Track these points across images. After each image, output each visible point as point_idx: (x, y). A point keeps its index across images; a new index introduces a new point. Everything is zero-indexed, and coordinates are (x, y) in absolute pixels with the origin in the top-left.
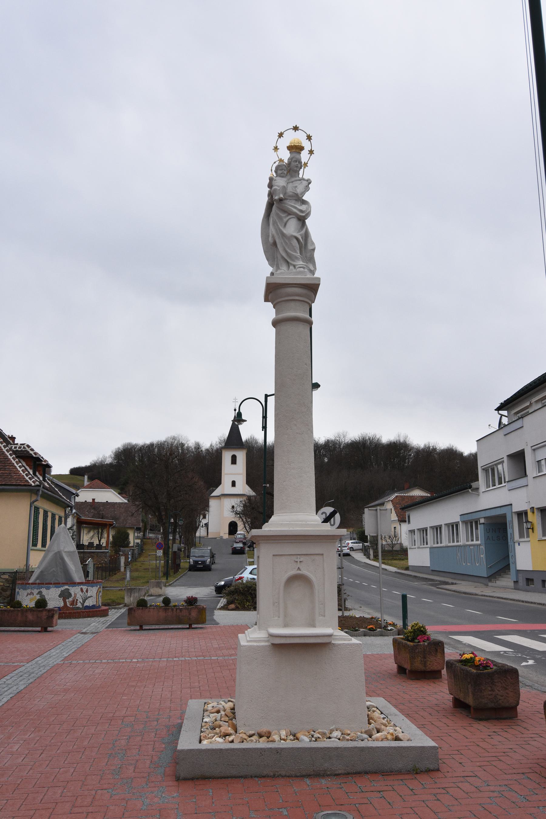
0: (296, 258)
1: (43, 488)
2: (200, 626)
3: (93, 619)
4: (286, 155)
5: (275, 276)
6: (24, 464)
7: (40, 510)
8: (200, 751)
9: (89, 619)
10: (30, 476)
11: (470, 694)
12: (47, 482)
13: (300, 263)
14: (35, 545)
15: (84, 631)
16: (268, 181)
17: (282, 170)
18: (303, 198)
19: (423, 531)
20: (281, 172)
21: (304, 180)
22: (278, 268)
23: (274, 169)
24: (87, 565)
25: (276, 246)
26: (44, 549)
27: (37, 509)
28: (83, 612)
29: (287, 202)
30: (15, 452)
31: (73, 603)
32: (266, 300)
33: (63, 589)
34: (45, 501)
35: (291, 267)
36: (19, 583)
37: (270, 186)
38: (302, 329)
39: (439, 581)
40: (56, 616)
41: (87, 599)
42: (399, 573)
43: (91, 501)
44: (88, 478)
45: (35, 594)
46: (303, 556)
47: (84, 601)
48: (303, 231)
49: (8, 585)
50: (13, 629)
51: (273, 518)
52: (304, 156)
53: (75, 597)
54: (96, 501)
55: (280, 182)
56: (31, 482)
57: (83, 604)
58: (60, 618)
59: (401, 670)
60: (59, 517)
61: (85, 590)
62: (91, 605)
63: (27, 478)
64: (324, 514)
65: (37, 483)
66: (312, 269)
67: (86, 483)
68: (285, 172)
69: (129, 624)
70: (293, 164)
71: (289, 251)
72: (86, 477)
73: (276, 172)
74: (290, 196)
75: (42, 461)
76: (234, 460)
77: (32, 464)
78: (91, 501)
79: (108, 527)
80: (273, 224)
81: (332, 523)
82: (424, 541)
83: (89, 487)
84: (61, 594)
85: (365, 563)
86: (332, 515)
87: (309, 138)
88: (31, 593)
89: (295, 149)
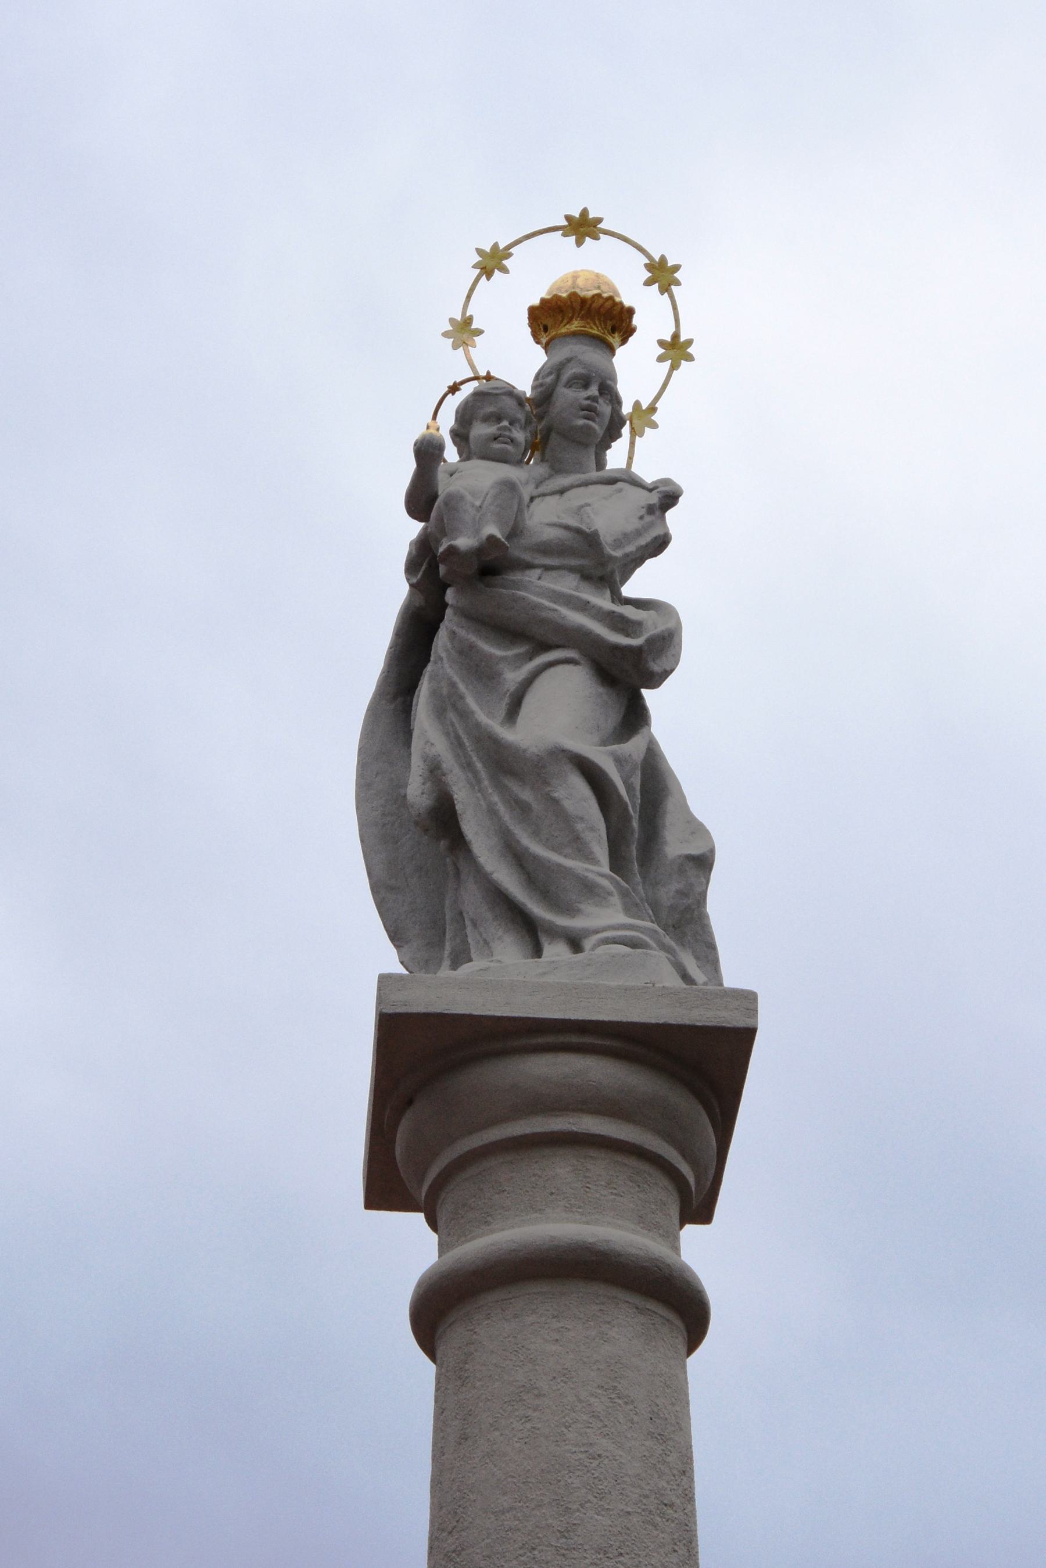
0: (590, 889)
4: (519, 362)
13: (606, 916)
17: (499, 418)
20: (491, 429)
21: (636, 482)
25: (458, 842)
37: (421, 500)
38: (623, 1329)
70: (567, 396)
71: (537, 849)
74: (545, 549)
80: (439, 713)
87: (662, 275)
89: (581, 320)
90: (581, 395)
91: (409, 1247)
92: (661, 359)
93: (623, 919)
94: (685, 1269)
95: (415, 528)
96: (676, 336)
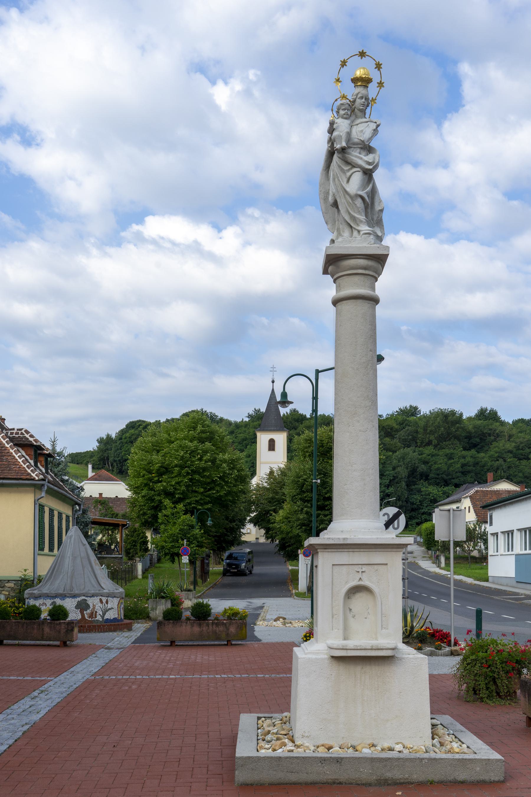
1: (48, 482)
2: (240, 642)
3: (115, 634)
5: (336, 244)
6: (24, 454)
7: (45, 507)
8: (259, 759)
9: (111, 633)
10: (32, 468)
12: (50, 475)
13: (364, 228)
14: (41, 549)
16: (328, 125)
19: (508, 534)
22: (339, 234)
26: (51, 553)
27: (41, 508)
28: (104, 626)
29: (350, 151)
30: (12, 440)
31: (93, 614)
32: (325, 272)
33: (79, 599)
34: (50, 497)
35: (355, 233)
37: (331, 130)
39: (525, 595)
40: (76, 630)
41: (107, 611)
43: (98, 496)
44: (93, 468)
46: (365, 566)
47: (104, 614)
48: (369, 188)
50: (28, 642)
51: (332, 525)
53: (94, 608)
54: (104, 496)
56: (34, 475)
57: (103, 617)
58: (80, 631)
60: (66, 516)
61: (104, 601)
62: (112, 618)
63: (29, 471)
64: (386, 516)
65: (41, 477)
66: (380, 234)
67: (90, 474)
68: (349, 113)
69: (159, 640)
72: (90, 466)
74: (354, 144)
75: (44, 450)
76: (272, 445)
77: (33, 453)
78: (98, 496)
79: (120, 528)
81: (396, 526)
82: (510, 546)
83: (92, 479)
86: (396, 516)
88: (44, 603)
91: (330, 291)
92: (378, 87)
93: (367, 228)
94: (377, 295)
96: (381, 81)
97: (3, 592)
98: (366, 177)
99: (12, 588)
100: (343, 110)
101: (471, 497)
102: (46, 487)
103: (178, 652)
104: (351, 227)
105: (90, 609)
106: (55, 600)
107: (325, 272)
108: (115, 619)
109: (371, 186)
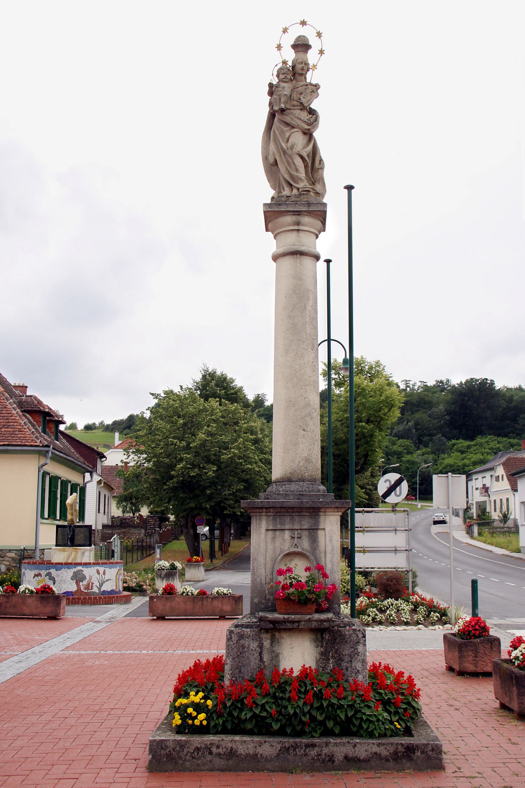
4: (290, 56)
11: (515, 698)
15: (98, 619)
16: (267, 89)
18: (312, 106)
21: (311, 85)
23: (275, 73)
24: (112, 542)
30: (20, 404)
33: (75, 570)
36: (25, 563)
40: (64, 602)
41: (104, 582)
42: (507, 556)
45: (43, 576)
47: (101, 585)
49: (15, 565)
52: (312, 56)
53: (90, 579)
55: (287, 88)
57: (99, 589)
58: (68, 604)
59: (450, 669)
64: (388, 482)
73: (278, 76)
77: (41, 420)
81: (398, 493)
84: (73, 576)
85: (467, 543)
86: (398, 483)
87: (319, 35)
89: (301, 46)
90: (301, 66)
95: (251, 397)
97: (4, 562)
98: (306, 138)
99: (13, 559)
100: (283, 74)
101: (504, 464)
102: (50, 454)
103: (172, 625)
104: (291, 185)
105: (87, 580)
106: (50, 571)
107: (267, 230)
108: (112, 590)
109: (311, 146)
